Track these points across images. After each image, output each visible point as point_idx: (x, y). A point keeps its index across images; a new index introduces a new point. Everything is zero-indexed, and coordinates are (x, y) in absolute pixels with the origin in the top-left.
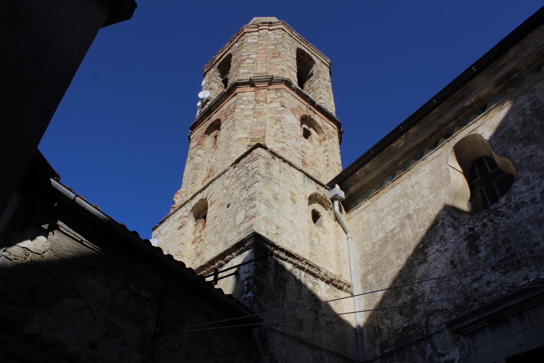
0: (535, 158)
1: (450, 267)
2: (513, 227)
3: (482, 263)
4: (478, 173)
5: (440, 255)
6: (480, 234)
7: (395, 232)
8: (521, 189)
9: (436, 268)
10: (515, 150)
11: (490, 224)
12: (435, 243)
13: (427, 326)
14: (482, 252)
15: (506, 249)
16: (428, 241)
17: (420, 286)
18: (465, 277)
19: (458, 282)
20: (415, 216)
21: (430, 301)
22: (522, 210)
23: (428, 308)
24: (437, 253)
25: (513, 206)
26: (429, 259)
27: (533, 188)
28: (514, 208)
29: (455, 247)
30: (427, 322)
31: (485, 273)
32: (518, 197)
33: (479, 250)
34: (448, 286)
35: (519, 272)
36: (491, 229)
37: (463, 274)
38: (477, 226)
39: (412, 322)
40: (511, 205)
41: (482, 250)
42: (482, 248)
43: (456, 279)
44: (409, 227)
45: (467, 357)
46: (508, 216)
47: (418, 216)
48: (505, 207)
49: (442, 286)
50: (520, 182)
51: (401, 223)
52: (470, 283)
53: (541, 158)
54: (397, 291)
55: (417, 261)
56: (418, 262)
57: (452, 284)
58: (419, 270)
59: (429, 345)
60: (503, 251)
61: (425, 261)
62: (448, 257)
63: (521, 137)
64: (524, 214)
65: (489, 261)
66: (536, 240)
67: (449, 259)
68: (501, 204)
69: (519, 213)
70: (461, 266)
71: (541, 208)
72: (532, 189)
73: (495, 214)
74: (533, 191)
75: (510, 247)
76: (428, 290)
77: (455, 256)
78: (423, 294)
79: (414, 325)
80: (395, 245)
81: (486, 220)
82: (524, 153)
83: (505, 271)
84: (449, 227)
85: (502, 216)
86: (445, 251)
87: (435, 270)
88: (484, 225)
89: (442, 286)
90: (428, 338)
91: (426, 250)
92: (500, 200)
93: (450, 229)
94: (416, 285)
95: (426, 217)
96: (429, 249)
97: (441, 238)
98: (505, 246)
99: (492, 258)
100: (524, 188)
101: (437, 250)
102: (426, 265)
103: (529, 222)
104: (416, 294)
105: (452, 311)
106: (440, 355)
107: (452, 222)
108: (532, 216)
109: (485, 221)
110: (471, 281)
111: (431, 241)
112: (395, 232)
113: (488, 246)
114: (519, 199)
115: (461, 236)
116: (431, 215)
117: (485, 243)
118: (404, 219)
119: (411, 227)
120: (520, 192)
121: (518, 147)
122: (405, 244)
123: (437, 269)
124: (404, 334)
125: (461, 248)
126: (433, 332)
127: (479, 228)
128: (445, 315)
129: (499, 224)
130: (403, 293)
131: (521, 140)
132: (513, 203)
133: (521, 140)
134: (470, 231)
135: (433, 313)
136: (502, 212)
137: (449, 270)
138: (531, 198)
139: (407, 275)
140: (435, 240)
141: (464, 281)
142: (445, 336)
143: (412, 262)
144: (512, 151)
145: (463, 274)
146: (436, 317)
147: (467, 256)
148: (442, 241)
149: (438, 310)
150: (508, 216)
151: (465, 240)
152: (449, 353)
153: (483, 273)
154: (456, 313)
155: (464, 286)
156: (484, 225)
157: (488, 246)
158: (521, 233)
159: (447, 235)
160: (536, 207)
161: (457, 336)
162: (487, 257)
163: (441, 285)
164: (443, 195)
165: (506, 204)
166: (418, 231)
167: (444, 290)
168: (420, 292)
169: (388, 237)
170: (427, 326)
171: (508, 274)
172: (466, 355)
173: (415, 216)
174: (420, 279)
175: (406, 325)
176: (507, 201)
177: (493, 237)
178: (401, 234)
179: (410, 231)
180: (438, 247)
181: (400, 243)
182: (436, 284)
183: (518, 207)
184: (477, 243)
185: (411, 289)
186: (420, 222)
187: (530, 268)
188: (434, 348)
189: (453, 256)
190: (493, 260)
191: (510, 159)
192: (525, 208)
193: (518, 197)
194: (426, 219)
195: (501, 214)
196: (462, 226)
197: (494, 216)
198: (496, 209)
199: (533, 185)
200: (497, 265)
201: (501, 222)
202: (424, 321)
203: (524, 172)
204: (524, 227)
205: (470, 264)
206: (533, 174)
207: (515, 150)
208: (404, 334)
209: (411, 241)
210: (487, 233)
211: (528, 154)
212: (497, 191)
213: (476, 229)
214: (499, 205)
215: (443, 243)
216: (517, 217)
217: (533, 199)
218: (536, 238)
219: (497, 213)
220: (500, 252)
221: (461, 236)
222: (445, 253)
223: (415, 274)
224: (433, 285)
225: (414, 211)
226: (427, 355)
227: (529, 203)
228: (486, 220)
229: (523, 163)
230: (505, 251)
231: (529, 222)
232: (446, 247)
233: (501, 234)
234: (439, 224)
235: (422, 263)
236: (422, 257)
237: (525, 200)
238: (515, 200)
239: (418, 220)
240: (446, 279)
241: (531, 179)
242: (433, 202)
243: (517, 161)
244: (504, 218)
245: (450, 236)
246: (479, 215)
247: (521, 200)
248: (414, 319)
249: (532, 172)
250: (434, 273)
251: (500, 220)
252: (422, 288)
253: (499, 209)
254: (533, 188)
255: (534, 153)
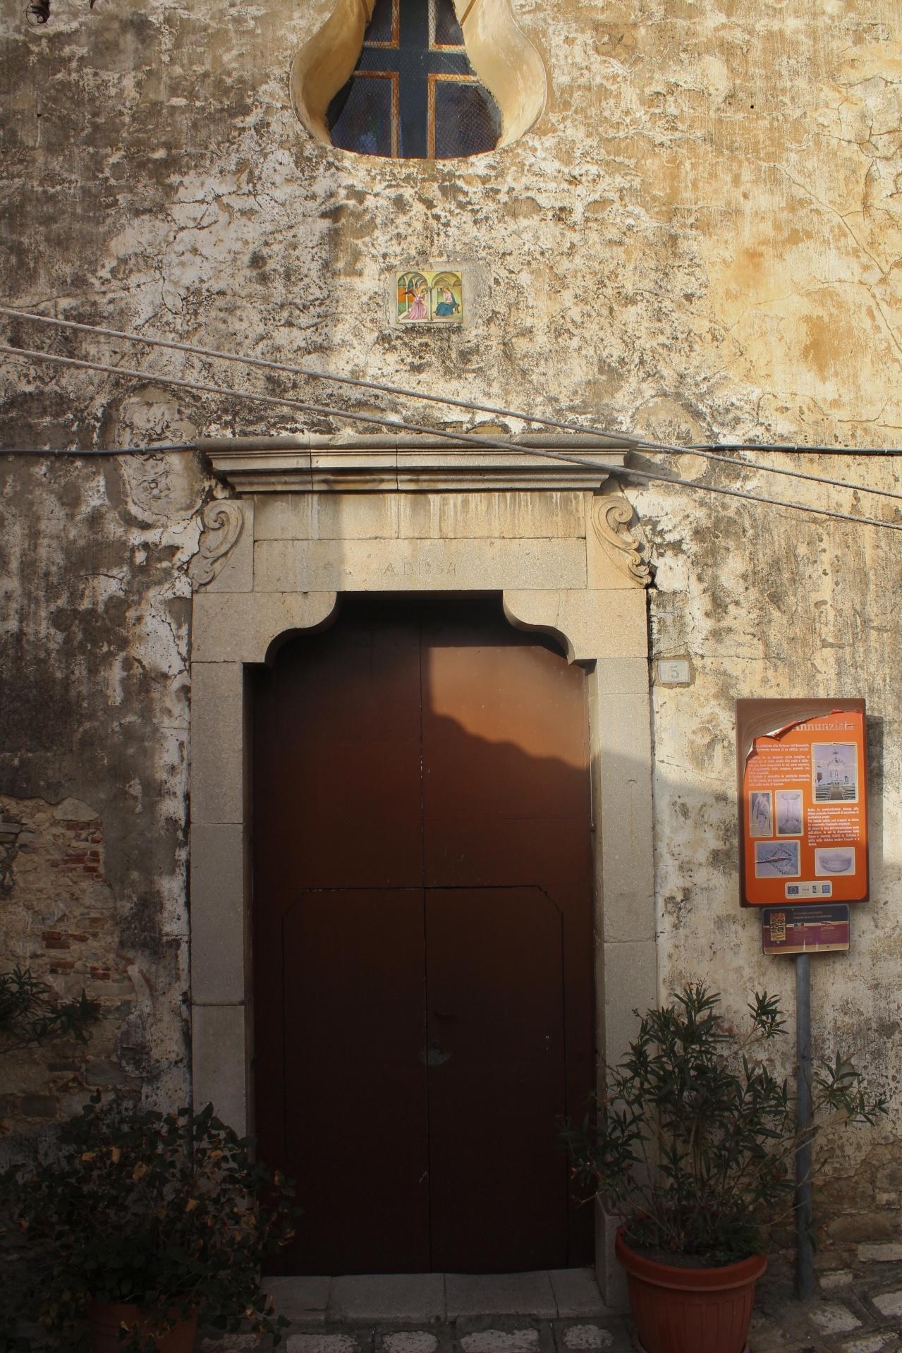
0: (612, 101)
1: (248, 272)
2: (484, 254)
3: (356, 309)
4: (394, 26)
5: (224, 217)
6: (378, 221)
7: (67, 51)
8: (543, 165)
9: (195, 251)
10: (568, 40)
11: (418, 208)
12: (215, 170)
13: (108, 420)
14: (365, 278)
15: (441, 305)
16: (191, 150)
17: (115, 283)
18: (289, 324)
19: (260, 329)
20: (167, 42)
21: (142, 348)
22: (524, 222)
23: (128, 367)
24: (214, 207)
25: (503, 197)
26: (178, 213)
27: (574, 180)
28: (505, 204)
29: (284, 221)
30: (113, 405)
31: (355, 342)
32: (524, 180)
33: (358, 266)
34: (223, 326)
35: (455, 384)
36: (418, 226)
37: (285, 314)
38: (376, 195)
39: (52, 387)
40: (498, 192)
41: (366, 271)
42: (371, 268)
43: (256, 317)
44: (130, 64)
45: (225, 554)
46: (480, 216)
47: (178, 45)
48: (480, 187)
49: (201, 319)
50: (547, 144)
51: (97, 33)
52: (299, 348)
53: (627, 113)
54: (22, 264)
55: (129, 196)
56: (132, 203)
57: (238, 326)
58: (129, 231)
59: (101, 481)
60: (431, 305)
61: (159, 210)
62: (249, 237)
63: (601, 17)
64: (525, 236)
65: (380, 315)
66: (529, 322)
67: (252, 248)
68: (470, 171)
69: (512, 226)
70: (285, 286)
71: (573, 246)
72: (570, 183)
73: (443, 190)
74: (572, 188)
75: (454, 304)
76: (146, 312)
77: (276, 247)
78: (124, 314)
79: (62, 402)
80: (55, 100)
81: (411, 191)
82: (588, 68)
83: (417, 361)
84: (282, 145)
85: (461, 206)
86: (243, 213)
87: (188, 256)
88: (400, 204)
89: (201, 319)
90: (104, 457)
91: (174, 179)
92: (472, 159)
93: (285, 156)
94: (104, 273)
95: (208, 67)
96: (186, 180)
97: (242, 166)
98: (441, 292)
99: (392, 308)
100: (551, 166)
101: (218, 197)
102: (162, 228)
103: (529, 263)
104: (94, 304)
105: (213, 406)
106: (131, 521)
107: (297, 137)
108: (542, 253)
109: (408, 192)
110: (303, 344)
111: (202, 156)
112: (67, 51)
113: (390, 268)
114: (527, 189)
115: (314, 197)
116: (229, 75)
117: (385, 256)
118: (116, 25)
119: (137, 68)
120: (535, 169)
121: (580, 38)
122: (95, 115)
123: (198, 259)
124: (13, 414)
125: (301, 230)
126: (126, 447)
127: (382, 202)
128: (188, 412)
129: (447, 225)
130: (43, 280)
131: (597, 26)
132: (505, 189)
133: (597, 26)
134: (348, 198)
135: (143, 385)
136: (466, 194)
137: (240, 279)
138: (558, 205)
139: (77, 226)
140: (219, 163)
141: (282, 336)
142: (166, 473)
143: (886, 1328)
144: (557, 40)
145: (285, 314)
146: (150, 405)
147: (316, 266)
148: (244, 177)
149: (165, 386)
150: (480, 216)
151: (324, 215)
152: (165, 527)
153: (349, 337)
154: (229, 418)
155: (278, 349)
156: (400, 204)
157: (390, 268)
158: (497, 282)
159: (266, 168)
160: (563, 235)
161: (207, 484)
162: (376, 301)
163: (196, 313)
164: (294, 29)
165: (485, 180)
166: (163, 96)
167: (202, 331)
168: (111, 302)
169: (30, 52)
170: (108, 420)
171: (423, 376)
172: (223, 550)
173: (167, 42)
174: (123, 261)
175: (30, 389)
176: (493, 173)
177: (413, 252)
178: (88, 70)
179: (129, 82)
180: (222, 189)
181: (79, 103)
182: (179, 304)
183: (512, 209)
184: (359, 242)
185: (79, 282)
186: (178, 70)
187: (490, 385)
188: (116, 492)
189: (266, 244)
190: (393, 318)
191: (545, 62)
192: (534, 221)
193: (524, 180)
194: (206, 75)
195: (461, 198)
196: (327, 169)
197: (438, 193)
198: (451, 175)
199: (576, 173)
200: (398, 338)
201: (453, 223)
202: (102, 400)
203: (568, 123)
204: (511, 272)
205: (318, 294)
206: (589, 142)
207: (568, 40)
208: (13, 414)
209: (127, 119)
210: (402, 230)
211: (598, 80)
212: (431, 115)
213: (370, 202)
214: (463, 170)
215: (246, 188)
216: (505, 233)
217: (562, 209)
218: (533, 316)
219: (450, 191)
220: (419, 303)
221: (314, 197)
222: (244, 220)
223: (110, 234)
224: (169, 301)
225: (168, 20)
226: (85, 510)
227: (550, 214)
228: (411, 191)
229: (577, 94)
230: (435, 308)
231: (529, 263)
232: (250, 202)
233: (441, 254)
234: (251, 120)
235: (145, 211)
236: (151, 192)
237: (542, 200)
238: (514, 185)
239: (172, 61)
240: (220, 302)
241: (578, 154)
242: (251, 33)
243: (562, 79)
244: (467, 217)
245: (278, 179)
246: (393, 164)
247: (529, 194)
248: (64, 382)
249: (589, 135)
250: (182, 264)
251: (450, 212)
252: (123, 294)
253: (460, 183)
254: (574, 180)
255: (614, 88)
